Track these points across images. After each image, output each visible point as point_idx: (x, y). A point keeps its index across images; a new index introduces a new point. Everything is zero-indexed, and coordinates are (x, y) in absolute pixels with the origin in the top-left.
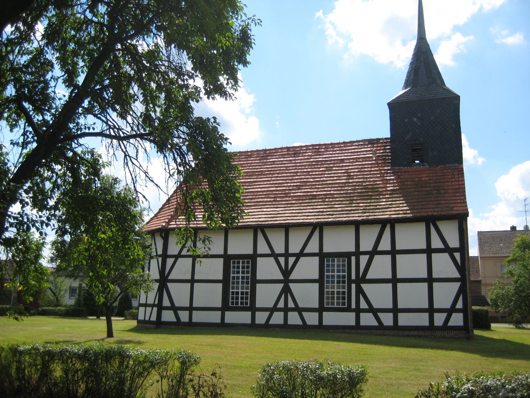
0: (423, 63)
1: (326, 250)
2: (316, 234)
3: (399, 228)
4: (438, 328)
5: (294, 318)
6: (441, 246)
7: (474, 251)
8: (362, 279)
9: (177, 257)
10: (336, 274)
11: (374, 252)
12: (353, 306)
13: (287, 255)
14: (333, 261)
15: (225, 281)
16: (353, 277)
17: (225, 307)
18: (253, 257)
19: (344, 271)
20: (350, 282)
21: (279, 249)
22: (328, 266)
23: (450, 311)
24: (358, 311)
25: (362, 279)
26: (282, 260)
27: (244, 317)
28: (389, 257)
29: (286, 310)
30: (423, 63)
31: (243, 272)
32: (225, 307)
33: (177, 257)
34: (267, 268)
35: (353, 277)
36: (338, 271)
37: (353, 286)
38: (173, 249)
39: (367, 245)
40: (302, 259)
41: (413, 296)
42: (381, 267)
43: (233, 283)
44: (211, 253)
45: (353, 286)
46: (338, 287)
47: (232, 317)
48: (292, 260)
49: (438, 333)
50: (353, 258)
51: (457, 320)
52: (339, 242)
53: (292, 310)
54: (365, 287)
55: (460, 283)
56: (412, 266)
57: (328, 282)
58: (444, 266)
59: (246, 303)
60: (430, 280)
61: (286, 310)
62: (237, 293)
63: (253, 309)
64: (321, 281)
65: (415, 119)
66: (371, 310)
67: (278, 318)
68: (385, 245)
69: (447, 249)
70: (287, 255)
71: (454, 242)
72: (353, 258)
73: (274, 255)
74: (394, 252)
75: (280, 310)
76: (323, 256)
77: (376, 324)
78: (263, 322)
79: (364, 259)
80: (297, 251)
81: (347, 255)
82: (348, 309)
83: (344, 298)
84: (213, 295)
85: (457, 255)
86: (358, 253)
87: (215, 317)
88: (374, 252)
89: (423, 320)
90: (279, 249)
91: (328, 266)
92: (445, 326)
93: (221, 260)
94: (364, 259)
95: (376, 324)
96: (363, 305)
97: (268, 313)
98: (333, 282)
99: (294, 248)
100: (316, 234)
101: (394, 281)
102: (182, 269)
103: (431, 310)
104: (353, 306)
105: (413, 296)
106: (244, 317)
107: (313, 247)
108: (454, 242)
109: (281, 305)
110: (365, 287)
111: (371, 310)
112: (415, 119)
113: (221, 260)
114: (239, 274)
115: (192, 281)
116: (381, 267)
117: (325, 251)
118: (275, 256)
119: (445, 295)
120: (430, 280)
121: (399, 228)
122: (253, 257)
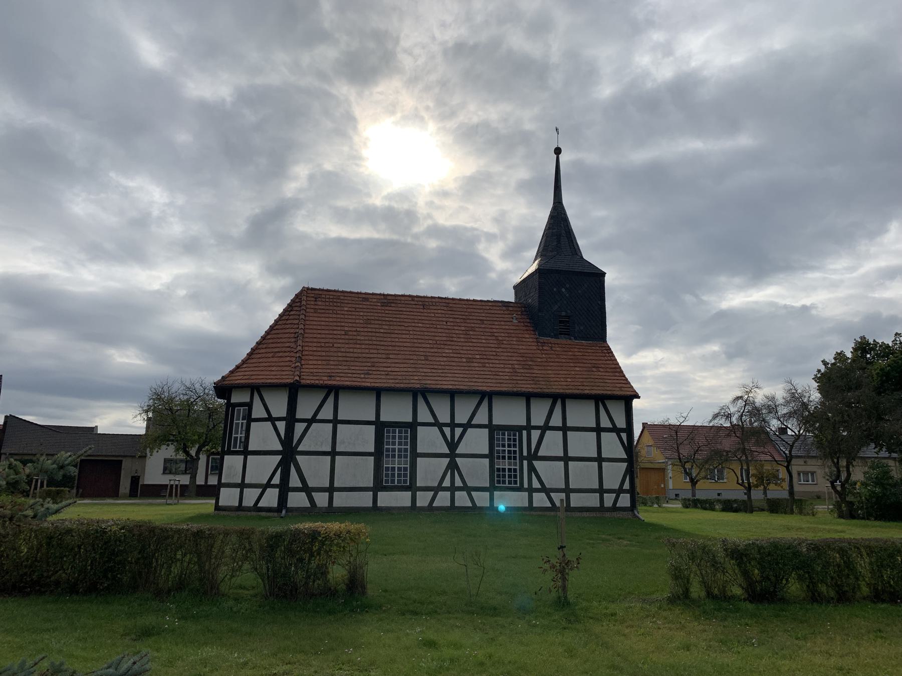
0: (559, 233)
1: (496, 422)
2: (485, 404)
3: (570, 404)
4: (248, 509)
5: (462, 499)
6: (608, 425)
7: (637, 430)
8: (534, 456)
9: (310, 422)
10: (397, 447)
11: (545, 428)
12: (526, 486)
13: (453, 425)
14: (504, 434)
15: (378, 454)
16: (525, 454)
17: (379, 486)
18: (413, 426)
19: (515, 446)
20: (522, 458)
21: (444, 418)
22: (498, 439)
23: (619, 491)
24: (531, 490)
25: (534, 456)
26: (447, 430)
27: (402, 499)
28: (330, 426)
29: (453, 489)
30: (559, 233)
31: (509, 446)
32: (379, 486)
33: (310, 422)
34: (430, 439)
35: (525, 454)
36: (400, 444)
37: (525, 463)
38: (305, 410)
39: (538, 419)
40: (470, 431)
41: (583, 475)
42: (552, 444)
43: (498, 476)
44: (646, 432)
45: (525, 463)
46: (510, 464)
47: (386, 499)
48: (458, 431)
49: (608, 515)
50: (525, 433)
51: (625, 501)
52: (509, 414)
53: (460, 489)
54: (537, 464)
55: (309, 505)
56: (582, 444)
57: (388, 456)
58: (612, 446)
59: (405, 481)
60: (566, 459)
61: (453, 489)
62: (504, 470)
63: (412, 487)
64: (490, 456)
65: (563, 290)
66: (544, 489)
67: (443, 499)
68: (327, 413)
69: (615, 429)
70: (453, 425)
71: (621, 423)
72: (525, 433)
73: (270, 419)
74: (335, 422)
75: (446, 489)
76: (493, 429)
77: (549, 505)
78: (426, 504)
79: (535, 434)
80: (464, 421)
81: (519, 429)
82: (520, 489)
83: (515, 476)
84: (361, 472)
85: (624, 436)
86: (529, 427)
87: (364, 500)
88: (545, 428)
89: (593, 500)
90: (444, 418)
91: (388, 437)
92: (614, 508)
93: (372, 428)
94: (535, 434)
95: (549, 505)
96: (458, 483)
97: (260, 490)
98: (394, 456)
99: (462, 417)
100: (485, 404)
101: (566, 459)
102: (317, 437)
103: (601, 491)
104: (526, 486)
105: (583, 475)
106: (402, 499)
107: (482, 417)
108: (621, 423)
109: (447, 483)
110: (537, 464)
111: (544, 489)
112: (563, 290)
113: (372, 428)
114: (395, 443)
115: (333, 453)
116: (552, 444)
117: (382, 419)
118: (440, 426)
119: (614, 474)
120: (600, 459)
121: (570, 404)
122: (413, 426)
